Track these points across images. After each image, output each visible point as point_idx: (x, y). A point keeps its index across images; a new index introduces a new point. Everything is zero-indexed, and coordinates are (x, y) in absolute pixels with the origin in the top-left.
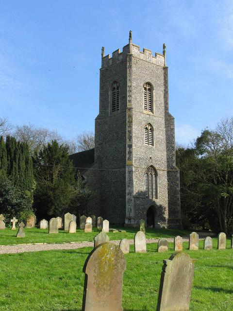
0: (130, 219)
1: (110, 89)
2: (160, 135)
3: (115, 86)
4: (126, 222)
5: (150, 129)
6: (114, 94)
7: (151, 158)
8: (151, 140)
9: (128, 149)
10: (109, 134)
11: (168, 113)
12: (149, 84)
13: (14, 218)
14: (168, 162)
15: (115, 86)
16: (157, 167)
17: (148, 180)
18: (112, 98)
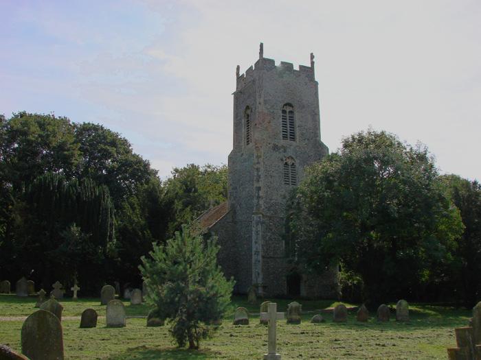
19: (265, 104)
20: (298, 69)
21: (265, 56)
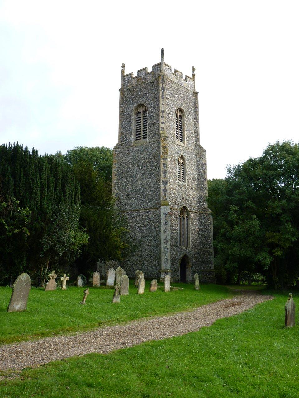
1: (133, 112)
2: (191, 170)
3: (141, 110)
5: (182, 162)
8: (182, 177)
9: (162, 187)
11: (199, 145)
12: (180, 110)
13: (65, 275)
14: (200, 202)
16: (189, 208)
17: (180, 223)
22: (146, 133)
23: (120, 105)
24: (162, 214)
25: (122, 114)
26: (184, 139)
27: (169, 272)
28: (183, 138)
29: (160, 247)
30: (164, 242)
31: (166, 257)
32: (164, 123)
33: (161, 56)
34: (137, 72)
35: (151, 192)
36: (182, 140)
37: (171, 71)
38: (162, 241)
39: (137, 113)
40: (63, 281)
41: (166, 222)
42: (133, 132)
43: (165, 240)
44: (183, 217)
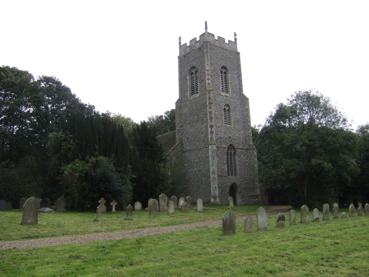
0: (215, 197)
3: (193, 71)
4: (212, 200)
6: (192, 79)
7: (230, 137)
10: (190, 116)
11: (243, 94)
12: (224, 67)
15: (193, 71)
16: (236, 146)
17: (228, 158)
18: (190, 83)
19: (211, 65)
20: (227, 43)
21: (209, 31)
22: (198, 89)
23: (179, 69)
24: (210, 151)
25: (180, 75)
26: (229, 90)
27: (217, 197)
28: (228, 90)
29: (209, 177)
30: (212, 174)
31: (214, 185)
32: (210, 79)
33: (205, 27)
34: (190, 42)
35: (203, 135)
36: (227, 92)
37: (214, 38)
38: (211, 173)
39: (191, 74)
40: (112, 205)
41: (213, 158)
42: (189, 89)
43: (213, 172)
44: (231, 153)
